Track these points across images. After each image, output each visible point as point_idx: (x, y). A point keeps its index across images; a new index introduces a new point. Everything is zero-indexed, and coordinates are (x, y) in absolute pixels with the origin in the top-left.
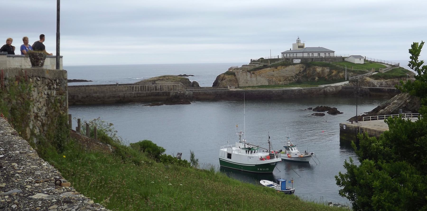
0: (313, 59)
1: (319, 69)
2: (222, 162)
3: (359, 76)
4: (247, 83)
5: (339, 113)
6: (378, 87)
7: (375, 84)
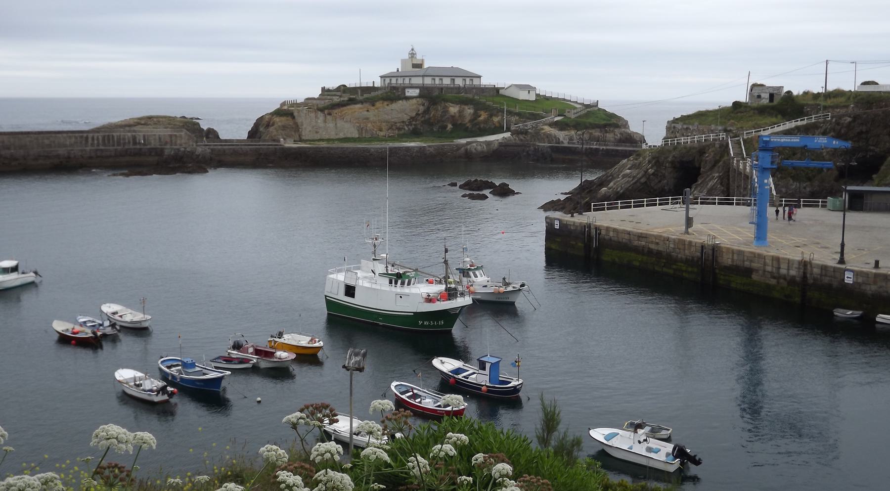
0: (442, 89)
1: (454, 110)
2: (331, 304)
3: (530, 124)
4: (317, 132)
5: (512, 193)
6: (566, 145)
7: (561, 139)
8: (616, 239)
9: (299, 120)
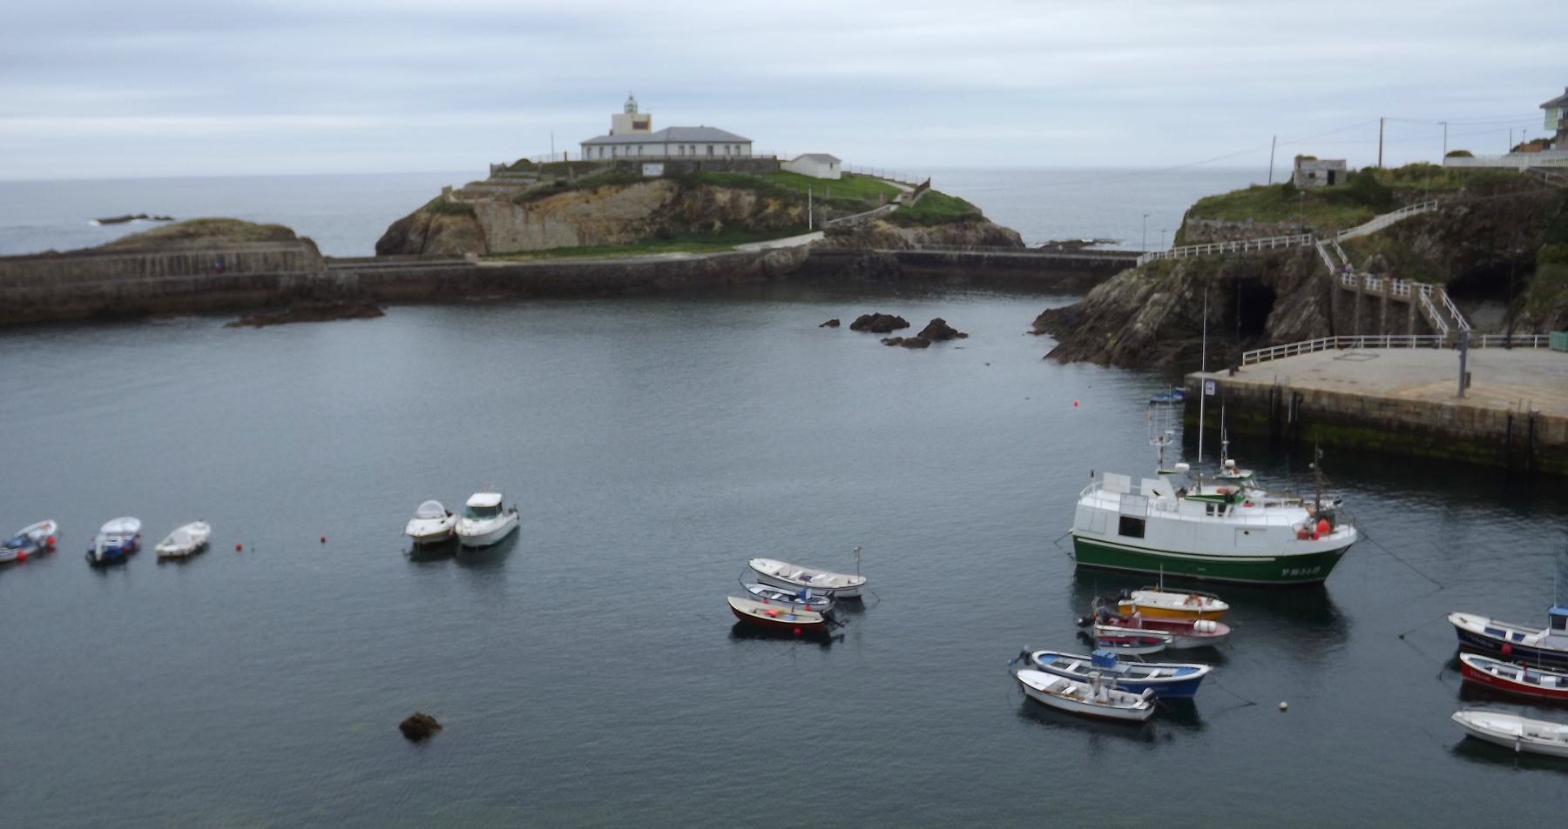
1: (723, 197)
3: (854, 218)
4: (514, 240)
7: (910, 242)
8: (1334, 408)
9: (484, 221)
